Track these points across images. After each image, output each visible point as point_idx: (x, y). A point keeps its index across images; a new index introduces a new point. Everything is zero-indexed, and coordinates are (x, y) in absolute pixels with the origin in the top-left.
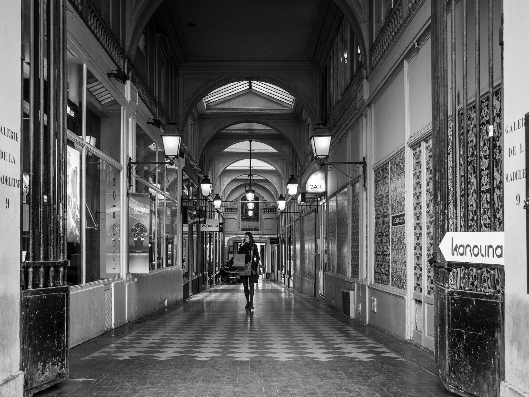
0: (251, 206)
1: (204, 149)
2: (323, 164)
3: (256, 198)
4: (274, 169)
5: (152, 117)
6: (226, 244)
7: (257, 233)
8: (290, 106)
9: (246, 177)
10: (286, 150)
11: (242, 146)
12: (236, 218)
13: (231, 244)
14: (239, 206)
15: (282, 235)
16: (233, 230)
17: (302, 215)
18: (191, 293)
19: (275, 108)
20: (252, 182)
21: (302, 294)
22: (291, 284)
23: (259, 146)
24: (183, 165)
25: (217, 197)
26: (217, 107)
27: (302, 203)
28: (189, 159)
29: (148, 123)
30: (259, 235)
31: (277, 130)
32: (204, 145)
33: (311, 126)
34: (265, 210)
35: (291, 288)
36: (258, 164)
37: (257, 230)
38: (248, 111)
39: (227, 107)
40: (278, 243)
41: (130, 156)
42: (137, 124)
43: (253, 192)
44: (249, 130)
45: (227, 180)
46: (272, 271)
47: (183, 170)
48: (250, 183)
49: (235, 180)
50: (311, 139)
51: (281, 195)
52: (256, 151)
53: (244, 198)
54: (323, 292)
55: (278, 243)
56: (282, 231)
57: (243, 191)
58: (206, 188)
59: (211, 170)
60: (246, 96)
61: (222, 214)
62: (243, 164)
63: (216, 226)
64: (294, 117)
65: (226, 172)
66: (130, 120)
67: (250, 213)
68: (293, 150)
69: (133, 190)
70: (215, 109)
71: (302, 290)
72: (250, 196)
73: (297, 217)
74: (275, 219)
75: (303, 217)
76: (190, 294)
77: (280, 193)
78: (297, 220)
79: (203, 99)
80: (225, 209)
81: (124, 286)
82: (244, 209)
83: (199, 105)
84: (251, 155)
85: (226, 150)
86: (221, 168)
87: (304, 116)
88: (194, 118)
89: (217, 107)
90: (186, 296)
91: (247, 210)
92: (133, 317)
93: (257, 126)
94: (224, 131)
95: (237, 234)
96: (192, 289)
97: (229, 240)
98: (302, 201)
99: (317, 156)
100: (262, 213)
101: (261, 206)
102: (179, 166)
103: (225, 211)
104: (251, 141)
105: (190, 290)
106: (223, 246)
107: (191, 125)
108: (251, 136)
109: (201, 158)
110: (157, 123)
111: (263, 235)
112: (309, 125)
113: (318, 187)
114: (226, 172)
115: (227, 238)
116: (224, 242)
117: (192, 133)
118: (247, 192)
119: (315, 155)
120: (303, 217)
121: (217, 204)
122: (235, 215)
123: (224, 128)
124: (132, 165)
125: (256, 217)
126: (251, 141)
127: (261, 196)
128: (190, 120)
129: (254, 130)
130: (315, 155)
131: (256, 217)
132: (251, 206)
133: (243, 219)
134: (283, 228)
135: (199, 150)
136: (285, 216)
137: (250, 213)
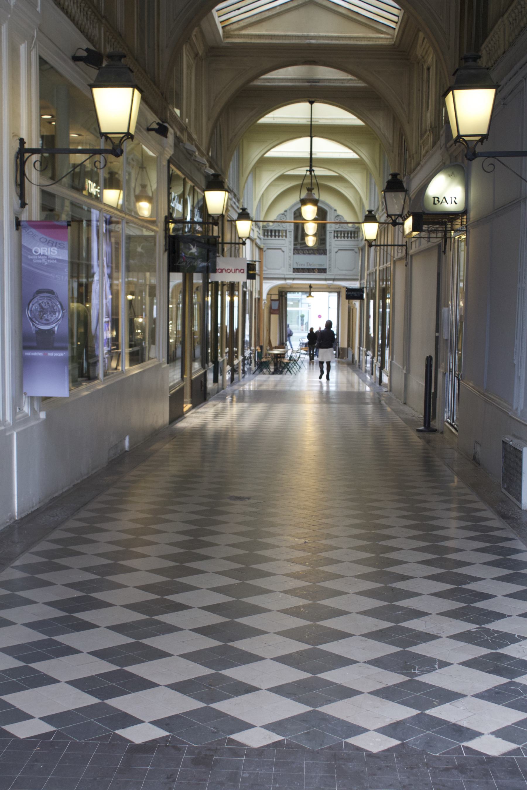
0: (311, 228)
1: (217, 120)
2: (462, 155)
3: (322, 214)
4: (356, 156)
5: (86, 44)
6: (264, 296)
7: (323, 277)
8: (390, 31)
9: (303, 171)
10: (381, 123)
11: (294, 113)
12: (283, 249)
13: (276, 297)
14: (290, 227)
15: (369, 282)
16: (277, 272)
17: (411, 252)
18: (187, 407)
19: (361, 35)
20: (314, 181)
21: (406, 409)
22: (385, 379)
23: (329, 113)
24: (169, 152)
25: (244, 215)
26: (243, 32)
27: (415, 233)
28: (185, 138)
29: (76, 59)
30: (326, 280)
31: (364, 81)
32: (218, 109)
33: (433, 71)
34: (338, 234)
35: (385, 386)
36: (326, 148)
37: (324, 271)
38: (307, 41)
39: (264, 32)
40: (361, 298)
41: (24, 135)
42: (41, 58)
43: (315, 202)
44: (309, 81)
45: (267, 178)
46: (349, 345)
47: (169, 162)
48: (310, 187)
49: (283, 178)
50: (446, 94)
51: (370, 212)
52: (322, 122)
53: (298, 214)
54: (452, 417)
55: (361, 298)
56: (369, 275)
57: (294, 199)
58: (216, 201)
59: (235, 157)
60: (302, 11)
61: (258, 241)
62: (297, 148)
63: (241, 271)
64: (399, 54)
65: (265, 162)
66: (23, 48)
67: (311, 241)
68: (395, 120)
69: (34, 211)
70: (240, 36)
71: (405, 399)
72: (309, 212)
73: (399, 253)
74: (357, 250)
75: (412, 256)
76: (185, 409)
77: (367, 208)
78: (400, 259)
79: (214, 11)
80: (264, 231)
81: (11, 436)
82: (300, 233)
83: (204, 24)
84: (311, 130)
85: (263, 120)
86: (254, 154)
87: (419, 51)
88: (197, 55)
89: (243, 32)
90: (177, 415)
91: (304, 235)
92: (35, 500)
93: (326, 73)
94: (258, 83)
95: (285, 279)
96: (192, 396)
97: (271, 290)
98: (414, 229)
99: (459, 136)
100: (333, 240)
101: (330, 228)
102: (161, 154)
103: (264, 235)
104: (311, 103)
105: (187, 399)
106: (259, 300)
107: (189, 67)
108: (312, 93)
109: (212, 133)
110: (92, 58)
111: (334, 280)
112: (428, 69)
113: (449, 201)
114: (265, 162)
115: (267, 286)
116: (260, 293)
117: (193, 86)
118: (304, 202)
119: (455, 135)
120: (412, 256)
121: (244, 228)
122: (282, 242)
123: (257, 77)
124: (26, 155)
125: (321, 248)
126: (311, 103)
127: (331, 208)
128: (186, 59)
129: (318, 81)
130: (455, 135)
131: (321, 248)
132: (311, 228)
133: (296, 251)
134: (372, 269)
135: (209, 119)
136: (376, 251)
137: (311, 241)
